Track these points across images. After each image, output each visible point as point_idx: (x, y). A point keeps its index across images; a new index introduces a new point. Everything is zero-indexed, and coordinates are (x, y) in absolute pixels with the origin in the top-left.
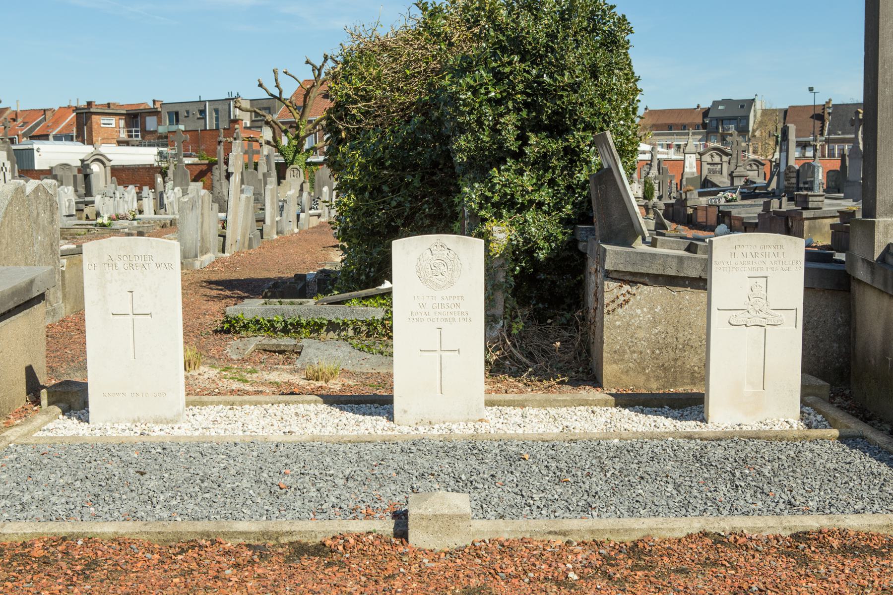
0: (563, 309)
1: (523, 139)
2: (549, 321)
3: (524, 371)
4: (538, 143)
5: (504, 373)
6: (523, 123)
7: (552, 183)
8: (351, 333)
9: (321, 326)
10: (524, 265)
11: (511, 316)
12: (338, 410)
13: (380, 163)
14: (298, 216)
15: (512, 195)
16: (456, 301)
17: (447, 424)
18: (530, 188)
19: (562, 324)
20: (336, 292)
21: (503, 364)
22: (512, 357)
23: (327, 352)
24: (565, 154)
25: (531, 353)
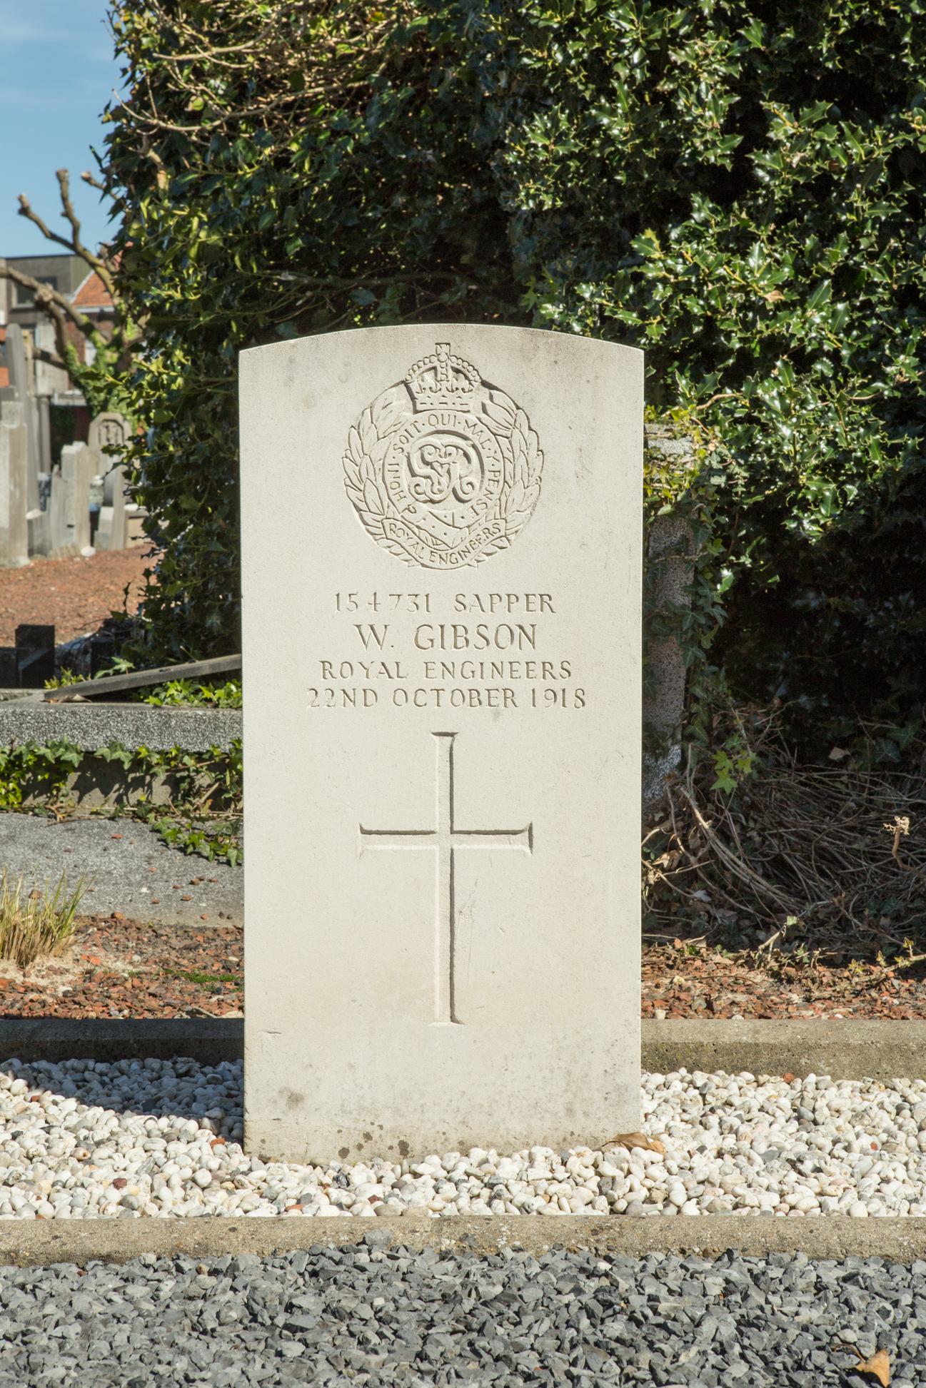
0: (885, 715)
1: (748, 124)
2: (837, 754)
3: (767, 928)
4: (798, 141)
5: (687, 933)
6: (749, 74)
7: (847, 281)
8: (161, 794)
9: (59, 770)
10: (746, 560)
11: (709, 729)
12: (20, 1084)
13: (268, 246)
14: (94, 517)
15: (709, 323)
16: (519, 615)
17: (478, 1154)
18: (772, 297)
19: (884, 765)
20: (124, 665)
21: (682, 901)
22: (715, 873)
23: (69, 859)
24: (895, 181)
25: (779, 862)
